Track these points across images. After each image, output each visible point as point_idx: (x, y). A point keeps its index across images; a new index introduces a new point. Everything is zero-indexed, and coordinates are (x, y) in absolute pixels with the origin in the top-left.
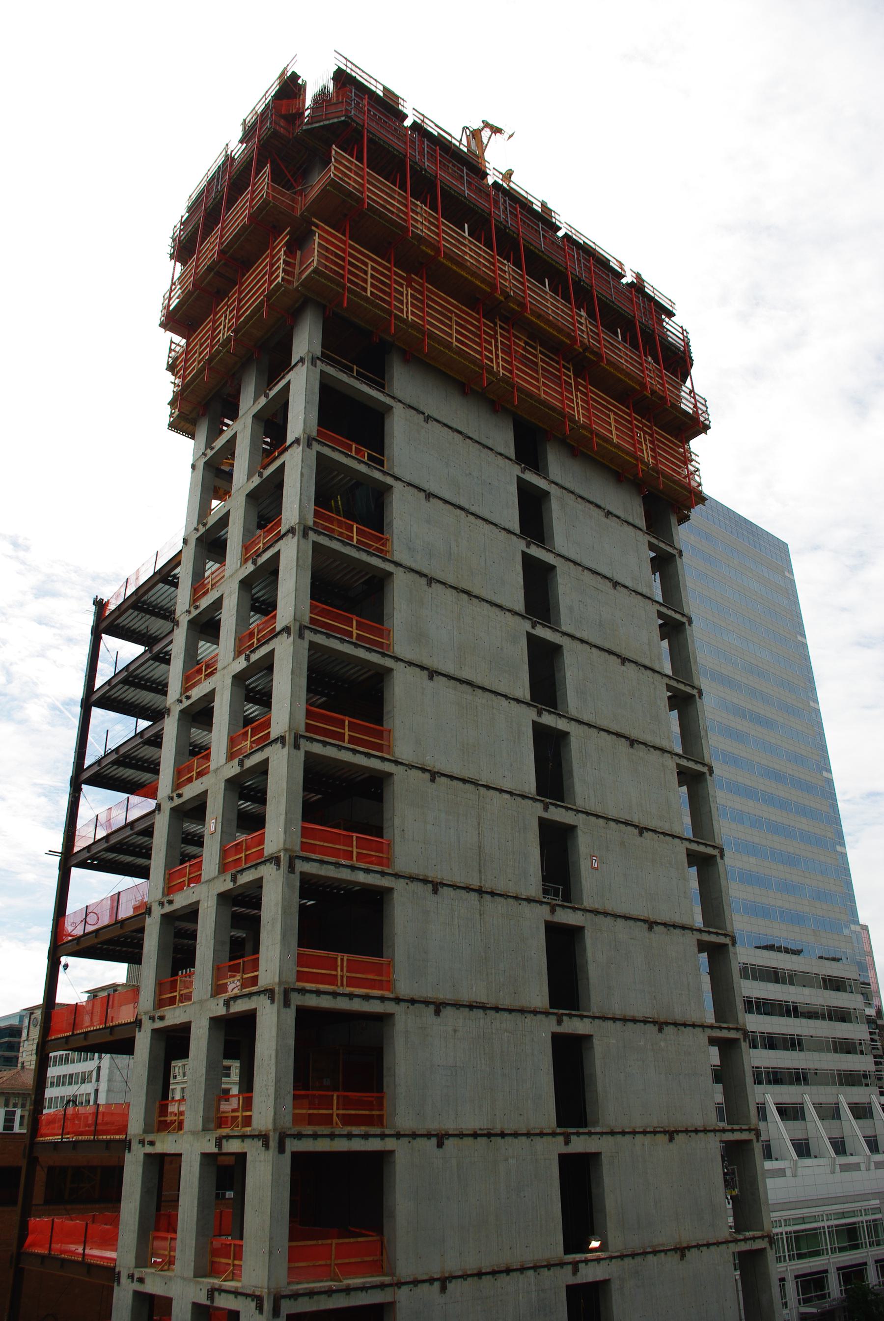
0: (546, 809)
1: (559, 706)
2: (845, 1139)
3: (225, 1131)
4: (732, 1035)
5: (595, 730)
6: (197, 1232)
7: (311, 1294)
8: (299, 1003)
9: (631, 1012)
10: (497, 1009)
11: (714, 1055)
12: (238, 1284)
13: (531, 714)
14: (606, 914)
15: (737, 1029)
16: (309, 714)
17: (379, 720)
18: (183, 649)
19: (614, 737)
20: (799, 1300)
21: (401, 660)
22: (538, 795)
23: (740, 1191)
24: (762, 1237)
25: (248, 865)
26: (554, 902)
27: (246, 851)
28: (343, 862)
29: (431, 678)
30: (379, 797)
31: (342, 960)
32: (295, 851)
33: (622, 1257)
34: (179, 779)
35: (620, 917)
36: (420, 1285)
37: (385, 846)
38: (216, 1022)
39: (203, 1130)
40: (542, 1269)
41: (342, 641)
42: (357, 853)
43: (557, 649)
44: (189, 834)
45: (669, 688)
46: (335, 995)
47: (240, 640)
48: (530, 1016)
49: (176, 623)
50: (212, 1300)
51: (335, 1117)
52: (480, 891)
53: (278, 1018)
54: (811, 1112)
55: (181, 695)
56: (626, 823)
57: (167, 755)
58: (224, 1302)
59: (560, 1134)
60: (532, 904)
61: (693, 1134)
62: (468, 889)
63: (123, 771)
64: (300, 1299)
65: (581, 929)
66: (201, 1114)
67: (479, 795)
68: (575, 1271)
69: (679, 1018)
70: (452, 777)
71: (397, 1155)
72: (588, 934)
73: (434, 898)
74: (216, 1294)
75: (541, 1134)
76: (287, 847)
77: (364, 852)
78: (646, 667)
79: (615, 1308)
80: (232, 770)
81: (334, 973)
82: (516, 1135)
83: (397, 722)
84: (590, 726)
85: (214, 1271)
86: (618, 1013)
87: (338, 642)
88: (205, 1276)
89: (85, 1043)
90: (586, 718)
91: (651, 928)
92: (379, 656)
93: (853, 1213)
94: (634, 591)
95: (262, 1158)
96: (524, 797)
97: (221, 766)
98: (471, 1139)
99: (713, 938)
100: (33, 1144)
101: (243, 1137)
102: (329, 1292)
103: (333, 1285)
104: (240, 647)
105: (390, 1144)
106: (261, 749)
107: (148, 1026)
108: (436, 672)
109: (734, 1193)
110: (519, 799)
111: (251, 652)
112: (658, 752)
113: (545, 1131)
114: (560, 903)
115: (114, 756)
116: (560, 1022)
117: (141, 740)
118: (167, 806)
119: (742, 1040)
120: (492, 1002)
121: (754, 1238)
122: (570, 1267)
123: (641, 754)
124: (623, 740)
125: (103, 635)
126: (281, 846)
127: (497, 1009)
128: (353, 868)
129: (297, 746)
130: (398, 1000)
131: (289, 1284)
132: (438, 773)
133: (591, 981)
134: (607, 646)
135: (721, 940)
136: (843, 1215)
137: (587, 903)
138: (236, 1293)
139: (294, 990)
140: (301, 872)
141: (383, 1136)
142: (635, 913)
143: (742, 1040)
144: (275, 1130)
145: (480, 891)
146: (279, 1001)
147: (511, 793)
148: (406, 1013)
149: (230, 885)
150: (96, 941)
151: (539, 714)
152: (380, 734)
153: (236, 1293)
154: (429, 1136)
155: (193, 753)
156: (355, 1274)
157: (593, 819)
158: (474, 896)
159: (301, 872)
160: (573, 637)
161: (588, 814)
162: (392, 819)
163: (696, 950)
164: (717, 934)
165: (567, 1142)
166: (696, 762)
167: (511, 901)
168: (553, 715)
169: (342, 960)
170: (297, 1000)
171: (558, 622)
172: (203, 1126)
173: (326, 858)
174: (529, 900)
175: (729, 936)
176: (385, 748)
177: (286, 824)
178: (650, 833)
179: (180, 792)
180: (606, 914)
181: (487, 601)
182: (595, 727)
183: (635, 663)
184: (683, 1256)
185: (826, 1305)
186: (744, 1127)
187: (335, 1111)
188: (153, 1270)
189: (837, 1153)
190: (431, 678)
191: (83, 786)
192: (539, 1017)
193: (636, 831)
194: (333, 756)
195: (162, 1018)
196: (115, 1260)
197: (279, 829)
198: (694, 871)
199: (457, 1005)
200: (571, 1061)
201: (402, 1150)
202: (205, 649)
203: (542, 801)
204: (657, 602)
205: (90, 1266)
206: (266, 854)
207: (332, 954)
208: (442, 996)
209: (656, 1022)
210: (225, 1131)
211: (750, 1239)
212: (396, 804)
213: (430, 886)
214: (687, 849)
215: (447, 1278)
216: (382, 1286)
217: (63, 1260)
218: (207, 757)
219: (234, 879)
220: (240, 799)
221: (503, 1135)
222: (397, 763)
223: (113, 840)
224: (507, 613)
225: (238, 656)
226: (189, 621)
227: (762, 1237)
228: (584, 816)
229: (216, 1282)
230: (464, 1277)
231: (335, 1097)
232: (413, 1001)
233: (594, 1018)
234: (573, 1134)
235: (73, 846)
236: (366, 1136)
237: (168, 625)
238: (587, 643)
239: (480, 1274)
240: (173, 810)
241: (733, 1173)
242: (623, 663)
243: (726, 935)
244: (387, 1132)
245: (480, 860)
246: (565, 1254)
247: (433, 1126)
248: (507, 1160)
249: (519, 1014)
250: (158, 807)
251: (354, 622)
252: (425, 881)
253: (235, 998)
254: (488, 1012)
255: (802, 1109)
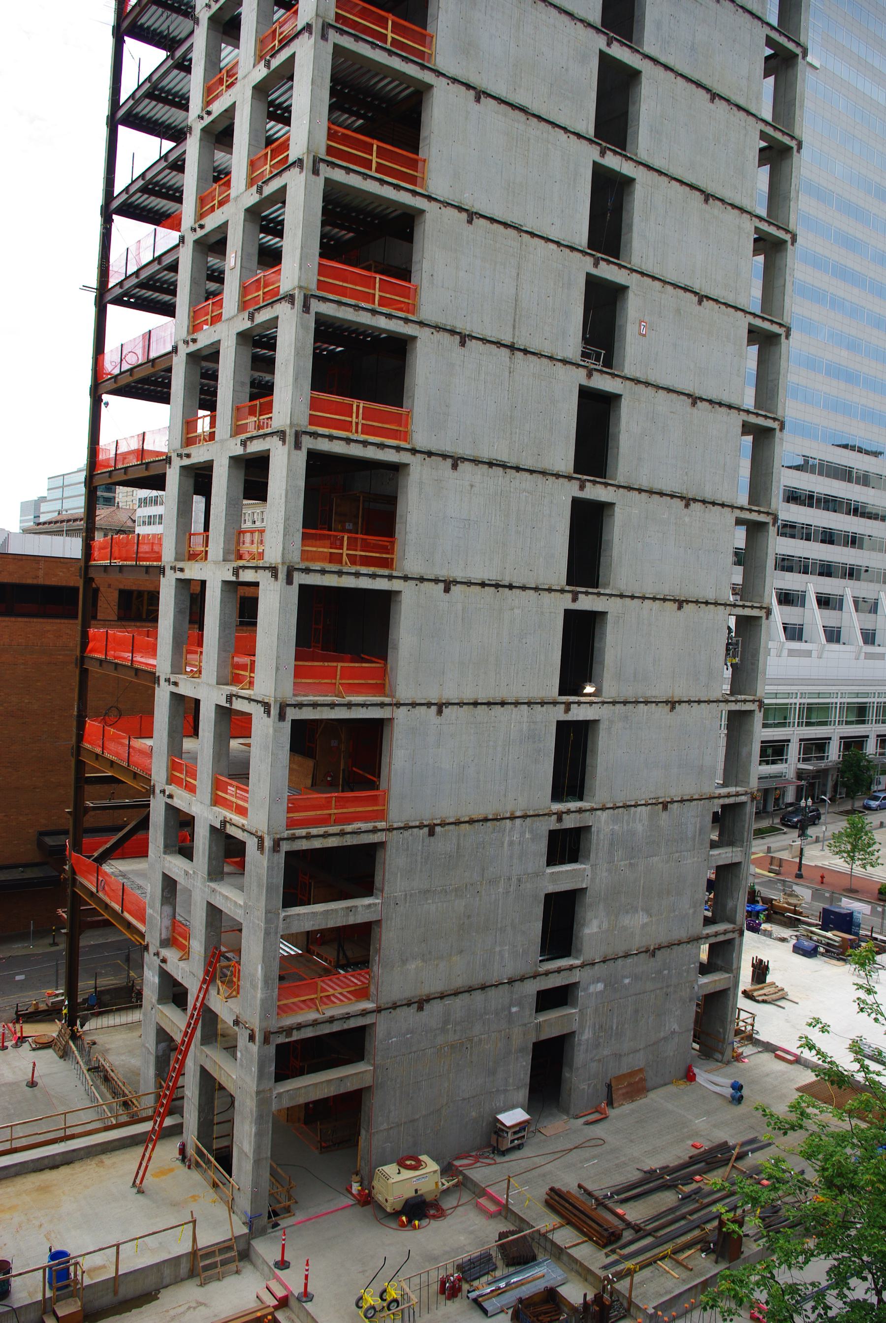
0: (596, 265)
1: (628, 147)
2: (877, 632)
3: (241, 563)
4: (762, 518)
5: (666, 179)
6: (219, 648)
7: (315, 705)
8: (311, 447)
9: (658, 486)
10: (518, 469)
11: (740, 538)
12: (245, 822)
13: (592, 153)
14: (647, 384)
15: (768, 514)
16: (331, 136)
17: (415, 149)
18: (204, 54)
19: (688, 189)
20: (799, 759)
21: (444, 75)
22: (589, 248)
23: (741, 660)
24: (753, 701)
25: (265, 303)
26: (593, 366)
27: (264, 288)
28: (363, 305)
29: (478, 100)
30: (409, 238)
31: (358, 407)
32: (310, 290)
33: (614, 703)
34: (202, 208)
35: (663, 388)
36: (417, 707)
37: (412, 291)
38: (235, 460)
39: (224, 561)
40: (535, 706)
41: (374, 45)
42: (380, 296)
43: (634, 75)
44: (214, 271)
45: (763, 136)
46: (348, 441)
47: (262, 41)
48: (552, 479)
49: (196, 21)
50: (231, 704)
51: (345, 556)
52: (512, 348)
53: (289, 459)
54: (849, 604)
55: (202, 110)
56: (686, 289)
57: (190, 181)
58: (239, 705)
59: (568, 591)
60: (568, 366)
61: (703, 606)
62: (499, 344)
63: (149, 200)
64: (304, 708)
65: (618, 397)
66: (222, 546)
67: (521, 243)
68: (567, 710)
69: (709, 497)
70: (492, 220)
71: (403, 595)
72: (625, 403)
73: (462, 350)
74: (234, 698)
75: (550, 590)
76: (302, 284)
77: (388, 296)
78: (739, 108)
79: (600, 743)
80: (252, 198)
81: (349, 419)
82: (524, 588)
83: (434, 151)
84: (660, 173)
85: (236, 680)
86: (645, 485)
87: (368, 47)
88: (227, 684)
89: (125, 478)
90: (657, 164)
91: (694, 404)
92: (418, 68)
93: (867, 695)
94: (742, 7)
95: (272, 588)
96: (572, 249)
97: (242, 195)
98: (478, 587)
99: (760, 421)
100: (87, 567)
101: (256, 568)
102: (332, 705)
103: (337, 700)
104: (261, 51)
105: (396, 585)
106: (279, 174)
107: (177, 463)
108: (484, 93)
109: (734, 661)
110: (567, 251)
111: (272, 56)
112: (736, 212)
113: (553, 588)
114: (599, 368)
115: (141, 183)
116: (582, 488)
117: (165, 164)
118: (191, 238)
119: (771, 524)
120: (513, 462)
121: (745, 701)
122: (562, 707)
123: (716, 212)
124: (698, 193)
125: (126, 38)
126: (296, 283)
127: (518, 469)
128: (374, 312)
129: (316, 172)
130: (414, 451)
131: (295, 695)
132: (476, 213)
133: (621, 450)
134: (695, 76)
135: (769, 423)
136: (857, 695)
137: (628, 371)
138: (250, 700)
139: (305, 433)
140: (316, 313)
141: (390, 577)
142: (679, 387)
143: (771, 524)
144: (283, 563)
145: (512, 348)
146: (290, 443)
147: (558, 243)
148: (422, 465)
149: (248, 324)
150: (131, 379)
151: (603, 154)
152: (414, 164)
153: (250, 700)
154: (436, 581)
155: (216, 179)
156: (359, 693)
157: (648, 281)
158: (505, 352)
159: (316, 313)
160: (655, 61)
161: (643, 274)
162: (421, 262)
163: (740, 430)
164: (766, 417)
165: (575, 600)
166: (779, 228)
167: (545, 361)
168: (618, 157)
169: (358, 407)
170: (308, 443)
171: (640, 42)
172: (224, 556)
173: (344, 300)
174: (565, 362)
175: (779, 420)
176: (419, 180)
177: (301, 259)
178: (711, 302)
179: (202, 222)
180: (647, 384)
181: (555, 6)
182: (666, 175)
183: (727, 101)
184: (673, 708)
185: (822, 765)
186: (756, 605)
187: (345, 551)
188: (185, 677)
189: (866, 642)
190: (478, 100)
191: (115, 217)
192: (561, 480)
193: (695, 299)
194: (357, 186)
195: (188, 456)
196: (155, 666)
197: (297, 265)
198: (754, 349)
199: (476, 461)
200: (588, 529)
201: (409, 594)
202: (227, 54)
203: (593, 255)
204: (768, 24)
205: (137, 670)
206: (281, 292)
207: (347, 400)
208: (460, 451)
209: (684, 498)
210: (241, 563)
211: (741, 701)
212: (426, 246)
213: (458, 338)
214: (749, 324)
215: (444, 704)
216: (382, 705)
217: (116, 664)
218: (228, 184)
219: (251, 317)
220: (261, 232)
221: (511, 587)
222: (430, 198)
223: (144, 275)
224: (578, 24)
225: (259, 62)
226: (209, 18)
227: (753, 701)
228: (639, 276)
229: (234, 689)
230: (461, 704)
231: (346, 538)
232: (430, 454)
233: (619, 487)
234: (582, 592)
235: (108, 282)
236: (373, 576)
237: (188, 24)
238: (672, 70)
239: (475, 704)
240: (197, 242)
241: (737, 644)
242: (712, 100)
243: (775, 419)
244: (395, 574)
245: (515, 314)
246: (559, 695)
247: (443, 573)
248: (513, 609)
249: (540, 476)
250: (182, 239)
251: (390, 23)
252: (452, 332)
253: (252, 438)
254: (508, 470)
255: (841, 601)
